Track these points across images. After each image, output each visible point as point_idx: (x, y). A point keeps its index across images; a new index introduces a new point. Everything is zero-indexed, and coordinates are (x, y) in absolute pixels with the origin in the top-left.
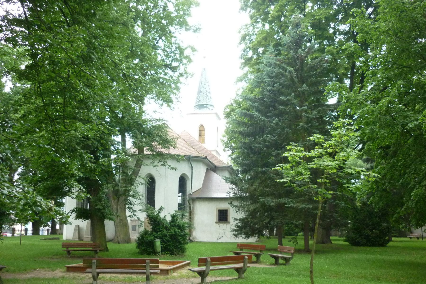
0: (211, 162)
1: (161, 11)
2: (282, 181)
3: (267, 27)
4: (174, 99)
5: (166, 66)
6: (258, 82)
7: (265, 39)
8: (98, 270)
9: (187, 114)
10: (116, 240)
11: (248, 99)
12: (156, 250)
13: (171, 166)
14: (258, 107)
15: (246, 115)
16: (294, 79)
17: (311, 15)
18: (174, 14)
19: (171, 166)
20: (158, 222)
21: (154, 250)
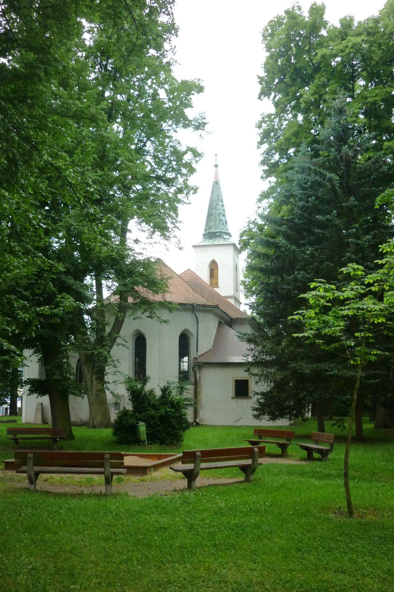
0: (224, 313)
1: (150, 102)
2: (301, 335)
3: (300, 117)
4: (169, 225)
5: (159, 178)
6: (285, 196)
7: (296, 134)
8: (37, 468)
9: (194, 246)
10: (91, 424)
11: (271, 221)
12: (140, 438)
13: (162, 318)
14: (285, 232)
15: (268, 244)
16: (336, 190)
17: (363, 97)
18: (168, 105)
19: (162, 318)
20: (143, 399)
21: (137, 438)
